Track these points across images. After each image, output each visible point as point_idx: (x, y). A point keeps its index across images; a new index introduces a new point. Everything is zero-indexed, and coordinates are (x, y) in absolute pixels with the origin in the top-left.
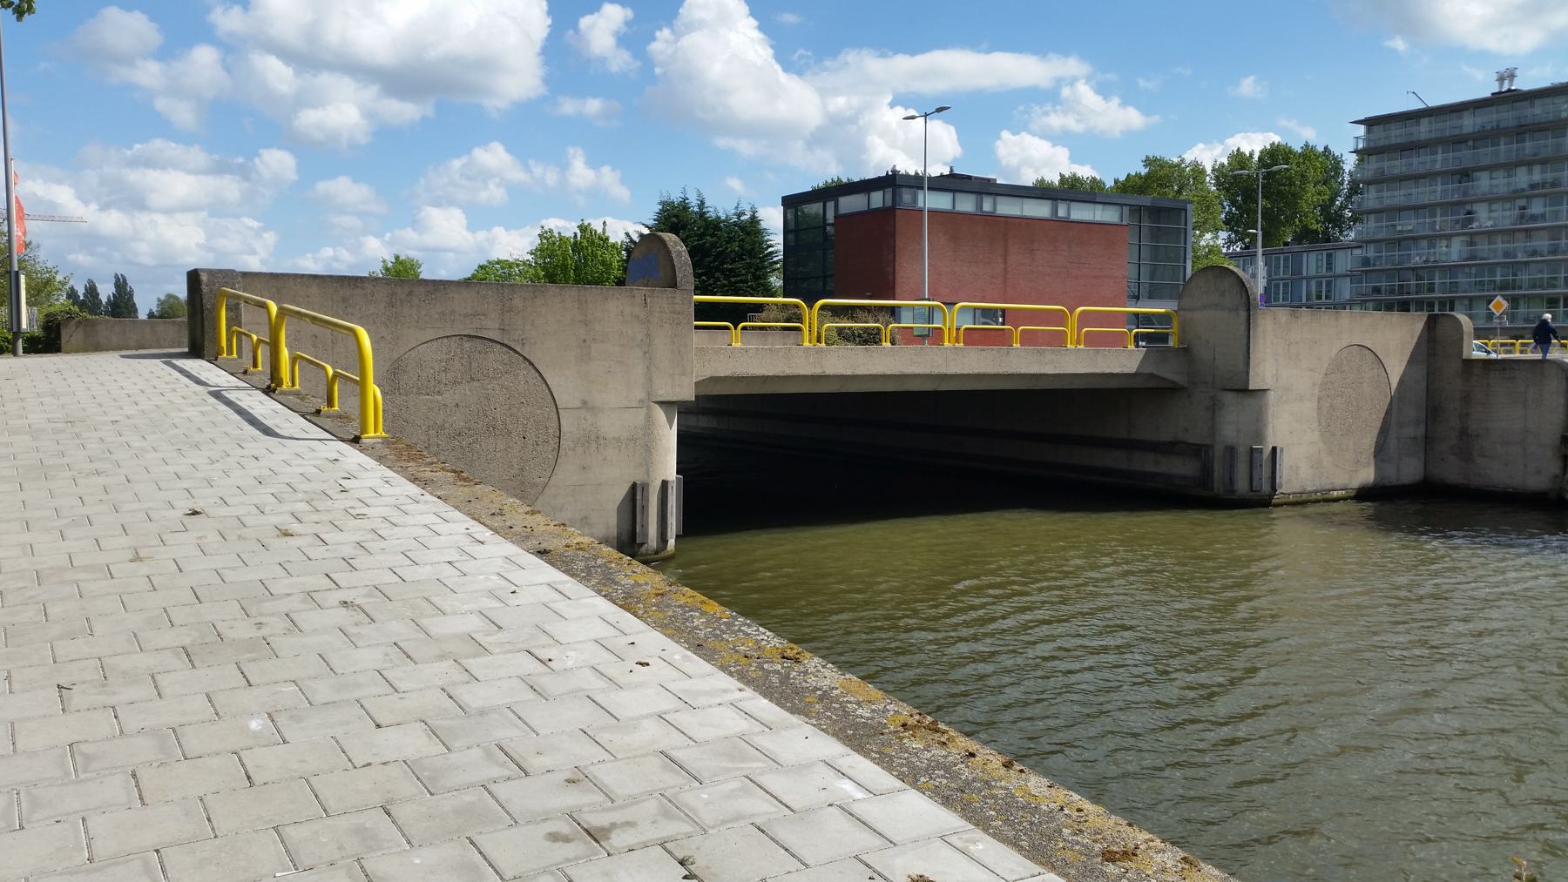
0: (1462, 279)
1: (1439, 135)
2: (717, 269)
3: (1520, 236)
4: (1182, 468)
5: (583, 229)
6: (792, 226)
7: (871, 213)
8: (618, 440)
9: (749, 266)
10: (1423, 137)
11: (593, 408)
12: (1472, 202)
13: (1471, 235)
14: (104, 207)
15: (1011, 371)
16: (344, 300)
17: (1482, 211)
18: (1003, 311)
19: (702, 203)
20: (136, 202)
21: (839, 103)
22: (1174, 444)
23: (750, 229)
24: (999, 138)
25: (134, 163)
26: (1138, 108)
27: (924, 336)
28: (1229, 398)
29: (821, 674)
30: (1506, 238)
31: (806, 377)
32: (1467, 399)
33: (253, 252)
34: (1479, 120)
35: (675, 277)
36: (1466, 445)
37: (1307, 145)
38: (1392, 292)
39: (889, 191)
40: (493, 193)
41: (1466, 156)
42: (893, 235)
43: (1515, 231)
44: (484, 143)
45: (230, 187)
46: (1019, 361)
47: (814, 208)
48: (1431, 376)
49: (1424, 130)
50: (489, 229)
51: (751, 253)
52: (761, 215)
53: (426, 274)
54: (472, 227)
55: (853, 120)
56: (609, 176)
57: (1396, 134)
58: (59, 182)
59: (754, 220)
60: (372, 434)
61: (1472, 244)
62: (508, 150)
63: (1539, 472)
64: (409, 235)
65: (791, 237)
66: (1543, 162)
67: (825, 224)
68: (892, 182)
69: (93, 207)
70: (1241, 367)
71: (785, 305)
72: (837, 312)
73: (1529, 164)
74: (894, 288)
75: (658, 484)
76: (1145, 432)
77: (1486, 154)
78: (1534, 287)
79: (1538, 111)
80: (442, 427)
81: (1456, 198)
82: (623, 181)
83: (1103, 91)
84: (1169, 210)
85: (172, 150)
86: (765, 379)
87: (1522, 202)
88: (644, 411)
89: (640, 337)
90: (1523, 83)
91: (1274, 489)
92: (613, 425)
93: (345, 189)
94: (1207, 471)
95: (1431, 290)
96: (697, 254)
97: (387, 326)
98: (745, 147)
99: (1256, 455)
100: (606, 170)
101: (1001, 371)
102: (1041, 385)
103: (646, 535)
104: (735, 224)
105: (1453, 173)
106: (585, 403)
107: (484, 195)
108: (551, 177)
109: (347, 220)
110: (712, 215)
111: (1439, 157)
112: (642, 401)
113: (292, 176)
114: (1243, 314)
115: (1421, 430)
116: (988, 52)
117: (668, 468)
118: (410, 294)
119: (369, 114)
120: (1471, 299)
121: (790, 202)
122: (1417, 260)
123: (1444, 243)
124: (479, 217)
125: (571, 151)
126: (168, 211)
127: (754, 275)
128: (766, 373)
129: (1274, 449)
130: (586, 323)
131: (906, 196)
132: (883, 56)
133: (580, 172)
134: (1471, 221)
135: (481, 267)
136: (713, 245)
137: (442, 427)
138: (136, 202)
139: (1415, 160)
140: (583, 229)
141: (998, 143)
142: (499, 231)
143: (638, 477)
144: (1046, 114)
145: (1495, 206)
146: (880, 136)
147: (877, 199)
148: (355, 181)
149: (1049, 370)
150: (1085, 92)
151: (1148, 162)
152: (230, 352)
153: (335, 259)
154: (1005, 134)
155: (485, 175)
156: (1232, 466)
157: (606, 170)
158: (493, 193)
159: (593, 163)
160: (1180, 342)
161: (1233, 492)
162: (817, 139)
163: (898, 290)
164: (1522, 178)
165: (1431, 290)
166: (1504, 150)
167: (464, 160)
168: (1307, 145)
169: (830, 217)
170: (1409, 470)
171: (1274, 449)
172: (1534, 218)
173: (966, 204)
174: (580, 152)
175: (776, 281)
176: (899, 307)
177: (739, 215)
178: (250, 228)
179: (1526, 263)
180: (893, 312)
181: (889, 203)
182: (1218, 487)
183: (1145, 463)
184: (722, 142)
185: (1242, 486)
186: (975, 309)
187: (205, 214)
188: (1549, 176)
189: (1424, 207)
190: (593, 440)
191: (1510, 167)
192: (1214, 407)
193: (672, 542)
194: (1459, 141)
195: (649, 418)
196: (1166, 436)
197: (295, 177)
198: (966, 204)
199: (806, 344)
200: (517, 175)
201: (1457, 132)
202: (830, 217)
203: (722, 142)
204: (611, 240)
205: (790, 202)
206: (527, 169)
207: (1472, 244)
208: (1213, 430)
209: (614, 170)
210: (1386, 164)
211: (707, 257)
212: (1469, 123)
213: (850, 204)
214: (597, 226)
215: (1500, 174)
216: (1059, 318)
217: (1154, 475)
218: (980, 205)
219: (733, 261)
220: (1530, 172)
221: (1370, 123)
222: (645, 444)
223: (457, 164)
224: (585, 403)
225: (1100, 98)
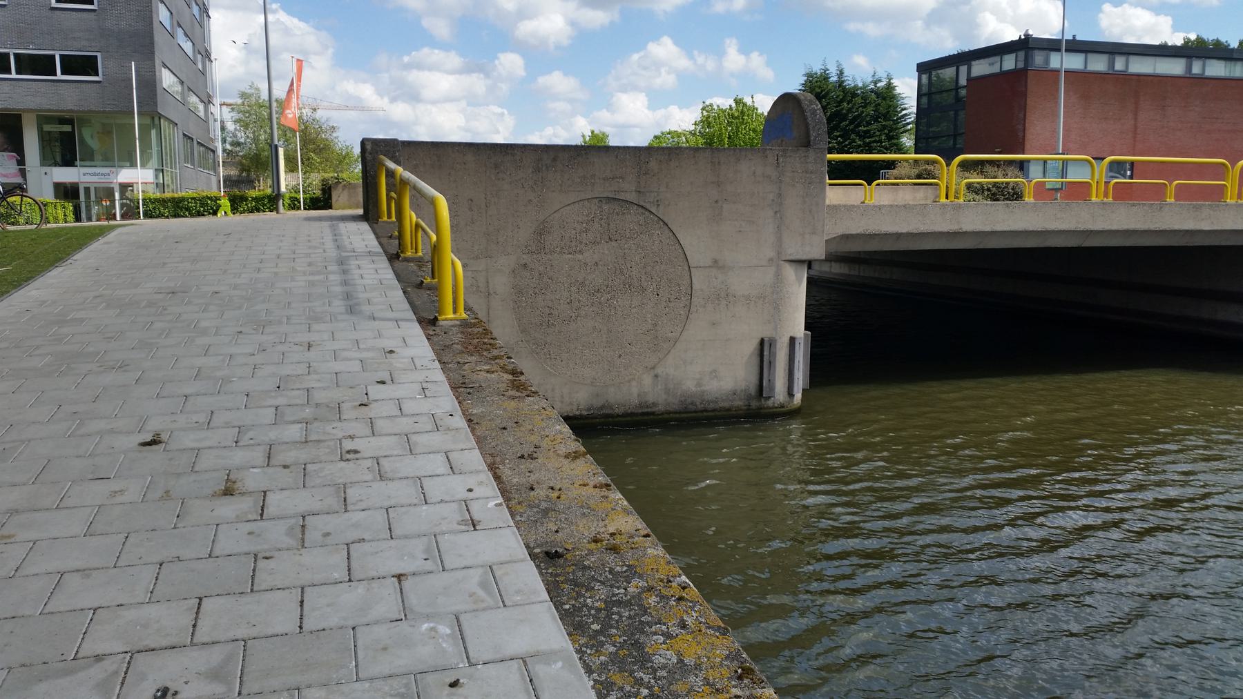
2: (853, 131)
5: (738, 101)
6: (925, 90)
7: (1003, 75)
8: (748, 298)
9: (884, 127)
11: (723, 267)
14: (393, 100)
15: (1163, 227)
16: (496, 166)
18: (1132, 163)
19: (841, 73)
20: (414, 97)
23: (886, 95)
24: (1100, 11)
25: (408, 67)
27: (1056, 190)
33: (498, 132)
35: (808, 135)
39: (1022, 54)
40: (666, 80)
42: (1025, 95)
44: (656, 38)
45: (477, 83)
46: (1173, 217)
47: (948, 73)
50: (666, 107)
51: (886, 116)
52: (895, 82)
53: (613, 142)
54: (652, 106)
56: (757, 60)
58: (364, 82)
59: (890, 87)
60: (451, 316)
62: (676, 43)
64: (604, 115)
65: (925, 100)
67: (957, 88)
68: (1025, 45)
69: (386, 100)
71: (916, 161)
72: (965, 166)
74: (1023, 144)
75: (786, 340)
80: (583, 284)
82: (768, 64)
85: (437, 55)
86: (898, 236)
88: (772, 270)
89: (771, 196)
92: (740, 284)
93: (558, 81)
96: (835, 120)
97: (534, 190)
98: (872, 29)
100: (755, 56)
102: (1198, 241)
103: (772, 389)
104: (872, 91)
106: (716, 261)
107: (658, 81)
108: (711, 65)
109: (561, 106)
110: (849, 83)
112: (771, 260)
113: (521, 72)
117: (796, 323)
118: (554, 160)
119: (572, 23)
121: (923, 68)
124: (657, 99)
125: (728, 41)
126: (434, 102)
127: (887, 135)
128: (900, 231)
130: (718, 184)
131: (1038, 58)
133: (734, 59)
135: (656, 137)
136: (849, 110)
137: (583, 284)
138: (414, 97)
140: (738, 101)
141: (1101, 15)
142: (674, 109)
143: (767, 333)
146: (992, 13)
147: (1009, 63)
148: (566, 75)
149: (1206, 226)
152: (389, 216)
153: (555, 135)
154: (1107, 7)
155: (658, 65)
157: (755, 56)
158: (666, 80)
159: (744, 50)
163: (1027, 146)
167: (642, 54)
169: (963, 81)
173: (1098, 64)
174: (734, 41)
175: (907, 141)
176: (1028, 161)
177: (876, 83)
178: (494, 114)
180: (1022, 166)
181: (1021, 65)
184: (852, 27)
187: (464, 103)
190: (723, 297)
193: (798, 396)
195: (778, 275)
197: (523, 73)
198: (1098, 64)
200: (683, 63)
202: (963, 81)
203: (852, 27)
204: (760, 111)
205: (923, 68)
206: (691, 57)
209: (761, 55)
211: (837, 123)
213: (980, 68)
214: (748, 100)
218: (1112, 64)
219: (869, 124)
222: (775, 302)
223: (636, 57)
224: (716, 261)
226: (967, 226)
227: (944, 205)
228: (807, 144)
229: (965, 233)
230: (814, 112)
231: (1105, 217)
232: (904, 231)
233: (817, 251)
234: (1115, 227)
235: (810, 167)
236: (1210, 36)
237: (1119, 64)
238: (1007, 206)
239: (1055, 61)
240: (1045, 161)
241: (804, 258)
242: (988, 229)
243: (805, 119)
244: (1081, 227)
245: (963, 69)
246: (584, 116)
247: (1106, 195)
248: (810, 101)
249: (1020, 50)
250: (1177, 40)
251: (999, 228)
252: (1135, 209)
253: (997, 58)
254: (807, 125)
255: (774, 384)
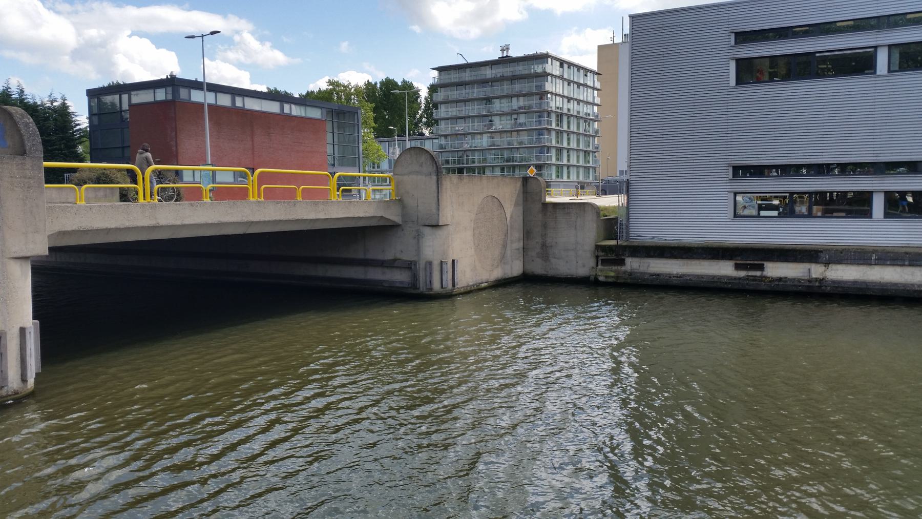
0: (488, 157)
1: (475, 78)
3: (515, 134)
4: (399, 277)
6: (95, 111)
10: (467, 79)
12: (492, 115)
13: (492, 133)
17: (496, 119)
19: (22, 91)
21: (93, 33)
22: (395, 260)
23: (63, 114)
26: (281, 50)
28: (427, 230)
29: (835, 214)
30: (509, 135)
31: (142, 227)
32: (545, 226)
34: (494, 72)
35: (23, 145)
36: (545, 252)
37: (404, 81)
38: (454, 163)
39: (170, 89)
41: (487, 91)
43: (512, 131)
48: (526, 213)
49: (467, 76)
52: (68, 103)
55: (103, 44)
57: (454, 77)
61: (492, 138)
63: (584, 266)
65: (95, 119)
66: (524, 95)
70: (434, 211)
73: (518, 96)
74: (176, 156)
76: (374, 254)
77: (498, 90)
78: (522, 160)
79: (521, 69)
81: (484, 113)
83: (262, 40)
84: (350, 112)
86: (108, 231)
87: (515, 116)
90: (514, 53)
91: (454, 285)
94: (415, 277)
95: (474, 162)
98: (24, 58)
99: (444, 266)
101: (291, 217)
104: (49, 108)
105: (483, 99)
111: (476, 90)
114: (434, 178)
115: (521, 244)
116: (189, 10)
120: (493, 167)
121: (91, 94)
122: (466, 146)
123: (479, 137)
129: (453, 261)
131: (183, 93)
132: (119, 6)
134: (492, 125)
139: (463, 91)
144: (225, 50)
145: (503, 118)
147: (161, 95)
150: (252, 42)
151: (330, 83)
156: (431, 276)
160: (396, 196)
161: (431, 289)
162: (80, 53)
164: (515, 104)
165: (474, 162)
166: (506, 88)
168: (404, 81)
170: (516, 269)
171: (453, 261)
172: (521, 125)
173: (225, 100)
176: (181, 171)
177: (52, 103)
179: (518, 148)
181: (170, 97)
182: (422, 288)
183: (375, 274)
184: (8, 54)
185: (436, 286)
186: (234, 172)
188: (527, 103)
189: (469, 117)
191: (510, 97)
192: (418, 236)
194: (484, 82)
196: (389, 256)
199: (141, 200)
201: (483, 77)
202: (125, 106)
205: (91, 94)
207: (492, 138)
208: (418, 250)
210: (449, 93)
212: (489, 73)
215: (515, 99)
216: (324, 180)
217: (381, 282)
220: (518, 101)
221: (441, 69)
225: (258, 43)
226: (163, 221)
227: (143, 205)
228: (23, 152)
229: (162, 226)
230: (27, 125)
231: (257, 212)
232: (113, 226)
233: (41, 248)
234: (267, 219)
235: (28, 173)
236: (281, 89)
237: (286, 107)
238: (192, 205)
239: (197, 96)
240: (193, 170)
241: (29, 254)
242: (179, 223)
243: (19, 131)
244: (245, 219)
245: (125, 97)
246: (75, 146)
247: (259, 196)
248: (22, 115)
249: (168, 86)
250: (263, 89)
251: (187, 222)
252: (279, 206)
253: (151, 91)
254: (21, 136)
255: (6, 374)
